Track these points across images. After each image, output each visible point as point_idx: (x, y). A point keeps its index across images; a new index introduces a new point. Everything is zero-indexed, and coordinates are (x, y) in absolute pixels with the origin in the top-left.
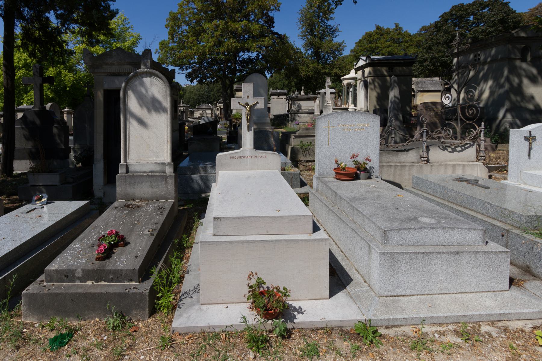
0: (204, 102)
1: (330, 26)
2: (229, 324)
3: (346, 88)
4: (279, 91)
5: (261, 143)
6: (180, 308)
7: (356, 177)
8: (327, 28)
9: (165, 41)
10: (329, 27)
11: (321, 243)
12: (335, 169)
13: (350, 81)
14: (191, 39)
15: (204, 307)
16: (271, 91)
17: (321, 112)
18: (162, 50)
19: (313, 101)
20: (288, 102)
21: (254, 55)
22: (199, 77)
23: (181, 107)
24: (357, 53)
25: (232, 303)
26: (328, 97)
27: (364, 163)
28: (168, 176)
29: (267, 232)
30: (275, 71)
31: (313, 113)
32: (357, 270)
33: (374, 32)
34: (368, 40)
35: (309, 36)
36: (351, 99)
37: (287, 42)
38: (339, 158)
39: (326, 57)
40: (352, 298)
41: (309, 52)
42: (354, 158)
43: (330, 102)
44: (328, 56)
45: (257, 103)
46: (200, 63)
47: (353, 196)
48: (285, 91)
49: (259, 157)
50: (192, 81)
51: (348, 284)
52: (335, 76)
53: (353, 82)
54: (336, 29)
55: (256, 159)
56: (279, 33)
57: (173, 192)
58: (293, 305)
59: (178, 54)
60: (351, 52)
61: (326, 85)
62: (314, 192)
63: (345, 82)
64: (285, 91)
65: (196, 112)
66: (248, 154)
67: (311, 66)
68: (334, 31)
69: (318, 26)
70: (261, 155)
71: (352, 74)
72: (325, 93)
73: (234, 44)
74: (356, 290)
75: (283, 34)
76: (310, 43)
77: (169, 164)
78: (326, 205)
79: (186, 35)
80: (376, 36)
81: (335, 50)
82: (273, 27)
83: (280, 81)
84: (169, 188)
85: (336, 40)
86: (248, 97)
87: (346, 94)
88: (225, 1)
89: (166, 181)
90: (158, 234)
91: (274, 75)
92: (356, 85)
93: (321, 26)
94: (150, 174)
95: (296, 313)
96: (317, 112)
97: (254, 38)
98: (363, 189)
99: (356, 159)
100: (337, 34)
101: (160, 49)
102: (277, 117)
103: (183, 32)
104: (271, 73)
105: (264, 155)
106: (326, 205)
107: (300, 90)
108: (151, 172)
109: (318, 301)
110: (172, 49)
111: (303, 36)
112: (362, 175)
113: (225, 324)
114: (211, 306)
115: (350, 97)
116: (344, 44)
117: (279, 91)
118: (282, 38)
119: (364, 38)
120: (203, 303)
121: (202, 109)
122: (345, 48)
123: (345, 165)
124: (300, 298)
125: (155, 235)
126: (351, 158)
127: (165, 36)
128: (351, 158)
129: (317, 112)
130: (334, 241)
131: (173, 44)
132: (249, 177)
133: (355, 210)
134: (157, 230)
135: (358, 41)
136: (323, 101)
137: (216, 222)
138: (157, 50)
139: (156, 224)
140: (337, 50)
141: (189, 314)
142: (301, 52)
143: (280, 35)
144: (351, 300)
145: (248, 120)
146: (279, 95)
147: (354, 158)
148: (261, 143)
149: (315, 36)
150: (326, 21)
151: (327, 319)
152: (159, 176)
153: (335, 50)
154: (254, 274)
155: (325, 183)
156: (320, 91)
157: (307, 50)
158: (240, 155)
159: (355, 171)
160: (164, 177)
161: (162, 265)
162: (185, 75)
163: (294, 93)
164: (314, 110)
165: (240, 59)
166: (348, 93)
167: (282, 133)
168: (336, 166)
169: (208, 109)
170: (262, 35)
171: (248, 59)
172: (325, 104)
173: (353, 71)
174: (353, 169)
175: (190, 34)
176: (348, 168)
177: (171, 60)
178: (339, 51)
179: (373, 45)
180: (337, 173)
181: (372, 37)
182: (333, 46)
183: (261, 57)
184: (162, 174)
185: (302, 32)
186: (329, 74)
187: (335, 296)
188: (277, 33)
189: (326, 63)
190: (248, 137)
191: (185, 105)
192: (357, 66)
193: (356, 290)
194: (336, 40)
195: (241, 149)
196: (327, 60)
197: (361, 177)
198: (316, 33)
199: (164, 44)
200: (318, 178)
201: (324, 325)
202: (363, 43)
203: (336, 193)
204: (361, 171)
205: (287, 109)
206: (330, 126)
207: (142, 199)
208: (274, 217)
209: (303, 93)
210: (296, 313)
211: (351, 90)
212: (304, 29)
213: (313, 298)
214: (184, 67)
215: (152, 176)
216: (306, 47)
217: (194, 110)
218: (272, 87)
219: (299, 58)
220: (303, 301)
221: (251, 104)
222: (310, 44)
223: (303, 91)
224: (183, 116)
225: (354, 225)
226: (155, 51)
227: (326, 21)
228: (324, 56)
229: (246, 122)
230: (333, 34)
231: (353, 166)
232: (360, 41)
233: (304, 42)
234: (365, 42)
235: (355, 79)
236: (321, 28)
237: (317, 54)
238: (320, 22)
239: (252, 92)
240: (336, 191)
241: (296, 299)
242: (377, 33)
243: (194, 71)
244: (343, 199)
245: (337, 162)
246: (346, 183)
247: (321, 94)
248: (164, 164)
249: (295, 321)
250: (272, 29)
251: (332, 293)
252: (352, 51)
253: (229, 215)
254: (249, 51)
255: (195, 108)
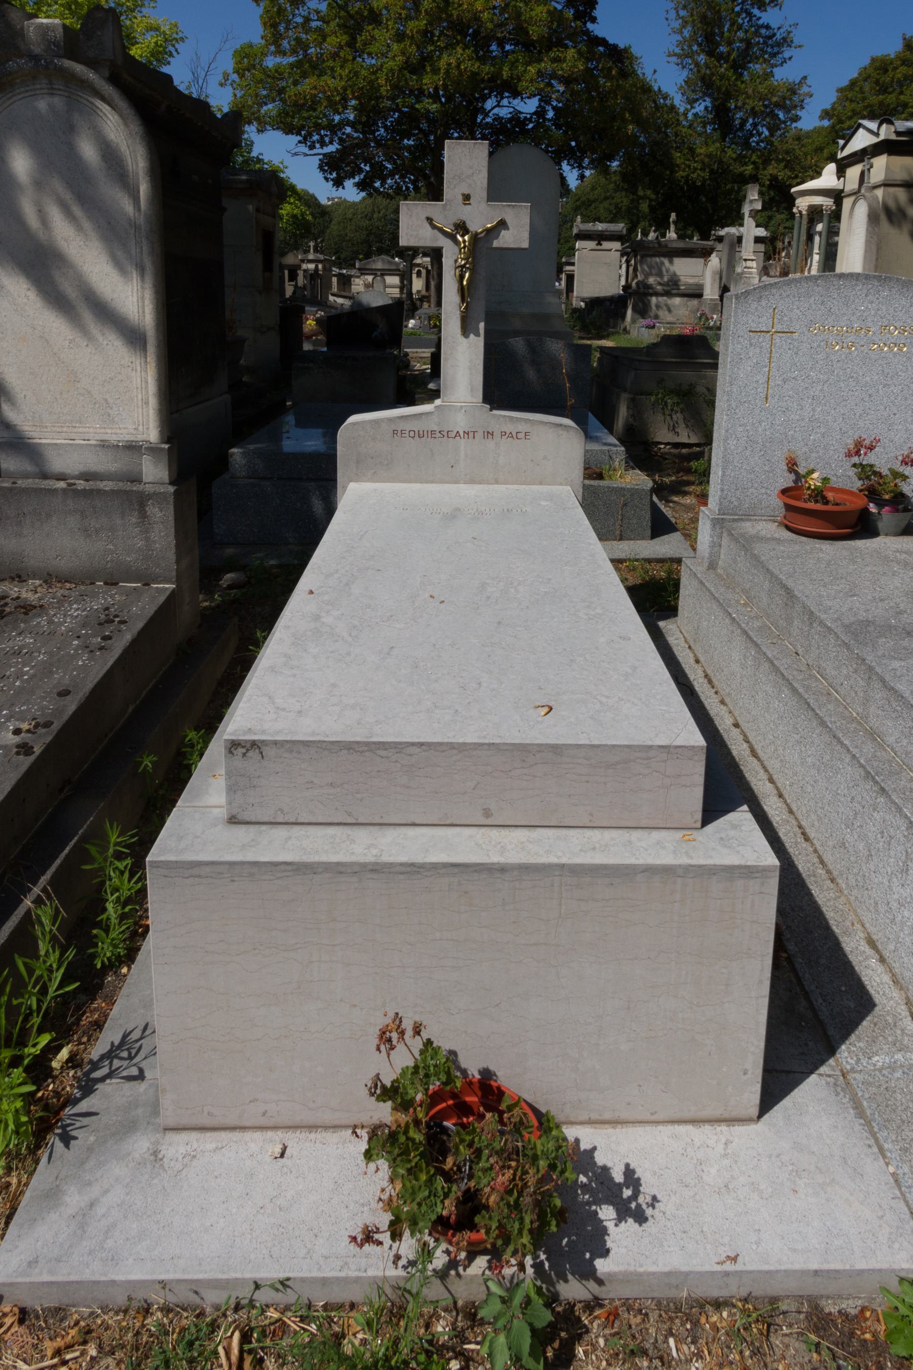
0: (381, 251)
1: (767, 27)
2: (271, 1272)
3: (805, 222)
4: (600, 227)
5: (505, 388)
6: (67, 1139)
7: (861, 526)
8: (757, 33)
9: (251, 46)
10: (763, 31)
11: (740, 883)
12: (784, 492)
13: (818, 200)
14: (333, 41)
15: (176, 1146)
16: (579, 225)
17: (725, 289)
18: (242, 76)
19: (702, 260)
20: (628, 262)
21: (529, 106)
22: (360, 171)
23: (310, 261)
24: (840, 122)
25: (312, 1128)
26: (748, 249)
27: (896, 475)
28: (150, 496)
29: (487, 813)
30: (592, 162)
31: (699, 296)
32: (872, 943)
33: (897, 57)
34: (877, 82)
35: (702, 58)
36: (816, 258)
37: (634, 71)
38: (800, 451)
39: (748, 126)
40: (860, 1112)
41: (700, 108)
42: (858, 453)
43: (754, 264)
44: (755, 125)
45: (502, 224)
46: (366, 124)
47: (862, 615)
48: (619, 227)
49: (503, 434)
50: (338, 183)
51: (848, 1027)
52: (771, 187)
53: (827, 203)
54: (784, 39)
55: (490, 444)
56: (611, 42)
57: (171, 555)
58: (600, 1159)
59: (292, 91)
60: (822, 118)
61: (746, 210)
62: (700, 570)
63: (803, 204)
64: (619, 227)
65: (357, 280)
66: (460, 422)
67: (701, 150)
68: (779, 44)
69: (732, 25)
70: (509, 428)
71: (828, 178)
72: (740, 239)
73: (467, 65)
74: (879, 1060)
75: (622, 46)
76: (703, 79)
77: (152, 450)
78: (745, 632)
79: (319, 29)
80: (903, 69)
81: (777, 105)
82: (594, 20)
83: (606, 198)
84: (154, 540)
85: (783, 74)
86: (467, 197)
87: (804, 237)
88: (479, 6)
89: (143, 515)
90: (48, 749)
91: (587, 173)
92: (836, 216)
93: (740, 27)
94: (81, 484)
95: (607, 1213)
96: (711, 292)
97: (533, 49)
98: (897, 582)
99: (870, 458)
100: (786, 55)
101: (236, 71)
102: (594, 303)
103: (307, 20)
104: (580, 167)
105: (522, 427)
106: (745, 632)
107: (662, 226)
108: (87, 476)
109: (707, 1128)
110: (278, 74)
111: (683, 56)
112: (887, 518)
113: (250, 1275)
114: (209, 1141)
115: (816, 250)
116: (805, 89)
117: (600, 227)
118: (619, 57)
119: (865, 76)
120: (171, 1122)
121: (373, 272)
122: (807, 100)
123: (825, 480)
124: (624, 1115)
125: (38, 750)
126: (849, 455)
127: (251, 29)
128: (849, 455)
129: (711, 292)
130: (771, 780)
131: (278, 59)
132: (453, 515)
133: (877, 685)
134: (56, 726)
135: (845, 83)
136: (731, 262)
137: (238, 762)
138: (226, 76)
139: (64, 693)
140: (781, 105)
141: (95, 1191)
142: (673, 108)
143: (615, 46)
144: (858, 1124)
145: (462, 290)
146: (600, 237)
147: (858, 453)
148: (505, 388)
149: (720, 57)
150: (756, 11)
151: (750, 1262)
152: (113, 491)
153: (777, 105)
154: (407, 1025)
155: (745, 543)
156: (722, 232)
157: (692, 102)
158: (432, 425)
159: (861, 502)
160: (134, 499)
161: (44, 890)
162: (316, 161)
163: (645, 234)
164: (701, 287)
165: (489, 120)
166: (810, 238)
167: (602, 349)
168: (787, 480)
169: (391, 272)
170: (554, 41)
171: (510, 120)
172: (739, 270)
173: (830, 169)
174: (851, 493)
175: (333, 24)
176: (833, 489)
177: (270, 108)
178: (787, 110)
179: (891, 99)
180: (788, 507)
181: (890, 74)
182: (773, 91)
183: (550, 114)
184: (128, 486)
185: (680, 44)
186: (754, 179)
187: (786, 1102)
188: (603, 42)
189: (746, 145)
190: (464, 360)
191: (322, 257)
192: (847, 151)
193: (879, 1060)
194: (783, 74)
195: (438, 402)
196: (752, 135)
197: (880, 525)
198: (723, 49)
199: (247, 56)
200: (717, 523)
201: (733, 1290)
202: (862, 91)
203: (788, 591)
204: (880, 504)
205: (623, 282)
206: (778, 327)
207: (50, 578)
208: (523, 749)
209: (672, 235)
210: (607, 1213)
211: (819, 227)
212: (686, 33)
213: (687, 1115)
214: (316, 137)
215: (86, 493)
216: (689, 93)
217: (353, 272)
218: (582, 215)
219: (667, 126)
220: (639, 1130)
221: (477, 225)
222: (704, 84)
223: (672, 227)
224: (313, 287)
225: (869, 748)
226: (220, 78)
227: (756, 11)
228: (744, 122)
229: (456, 299)
230: (774, 55)
231: (857, 484)
232: (853, 83)
233: (685, 74)
234: (867, 88)
235: (837, 196)
236: (740, 34)
237: (721, 116)
238: (738, 14)
239: (481, 179)
240: (790, 583)
241: (607, 1116)
242: (904, 62)
243: (343, 153)
244: (822, 623)
245: (792, 466)
246: (827, 547)
247: (726, 241)
248: (132, 448)
249: (602, 1266)
250: (590, 26)
251: (778, 1081)
252: (826, 114)
253: (305, 729)
254: (516, 94)
255: (353, 266)
